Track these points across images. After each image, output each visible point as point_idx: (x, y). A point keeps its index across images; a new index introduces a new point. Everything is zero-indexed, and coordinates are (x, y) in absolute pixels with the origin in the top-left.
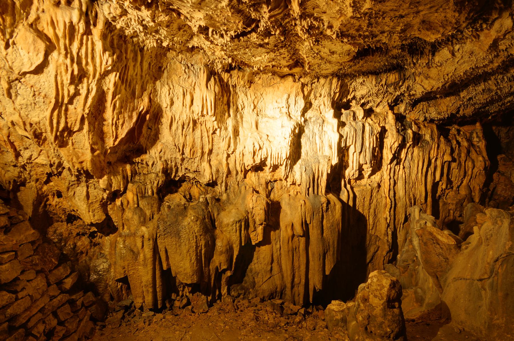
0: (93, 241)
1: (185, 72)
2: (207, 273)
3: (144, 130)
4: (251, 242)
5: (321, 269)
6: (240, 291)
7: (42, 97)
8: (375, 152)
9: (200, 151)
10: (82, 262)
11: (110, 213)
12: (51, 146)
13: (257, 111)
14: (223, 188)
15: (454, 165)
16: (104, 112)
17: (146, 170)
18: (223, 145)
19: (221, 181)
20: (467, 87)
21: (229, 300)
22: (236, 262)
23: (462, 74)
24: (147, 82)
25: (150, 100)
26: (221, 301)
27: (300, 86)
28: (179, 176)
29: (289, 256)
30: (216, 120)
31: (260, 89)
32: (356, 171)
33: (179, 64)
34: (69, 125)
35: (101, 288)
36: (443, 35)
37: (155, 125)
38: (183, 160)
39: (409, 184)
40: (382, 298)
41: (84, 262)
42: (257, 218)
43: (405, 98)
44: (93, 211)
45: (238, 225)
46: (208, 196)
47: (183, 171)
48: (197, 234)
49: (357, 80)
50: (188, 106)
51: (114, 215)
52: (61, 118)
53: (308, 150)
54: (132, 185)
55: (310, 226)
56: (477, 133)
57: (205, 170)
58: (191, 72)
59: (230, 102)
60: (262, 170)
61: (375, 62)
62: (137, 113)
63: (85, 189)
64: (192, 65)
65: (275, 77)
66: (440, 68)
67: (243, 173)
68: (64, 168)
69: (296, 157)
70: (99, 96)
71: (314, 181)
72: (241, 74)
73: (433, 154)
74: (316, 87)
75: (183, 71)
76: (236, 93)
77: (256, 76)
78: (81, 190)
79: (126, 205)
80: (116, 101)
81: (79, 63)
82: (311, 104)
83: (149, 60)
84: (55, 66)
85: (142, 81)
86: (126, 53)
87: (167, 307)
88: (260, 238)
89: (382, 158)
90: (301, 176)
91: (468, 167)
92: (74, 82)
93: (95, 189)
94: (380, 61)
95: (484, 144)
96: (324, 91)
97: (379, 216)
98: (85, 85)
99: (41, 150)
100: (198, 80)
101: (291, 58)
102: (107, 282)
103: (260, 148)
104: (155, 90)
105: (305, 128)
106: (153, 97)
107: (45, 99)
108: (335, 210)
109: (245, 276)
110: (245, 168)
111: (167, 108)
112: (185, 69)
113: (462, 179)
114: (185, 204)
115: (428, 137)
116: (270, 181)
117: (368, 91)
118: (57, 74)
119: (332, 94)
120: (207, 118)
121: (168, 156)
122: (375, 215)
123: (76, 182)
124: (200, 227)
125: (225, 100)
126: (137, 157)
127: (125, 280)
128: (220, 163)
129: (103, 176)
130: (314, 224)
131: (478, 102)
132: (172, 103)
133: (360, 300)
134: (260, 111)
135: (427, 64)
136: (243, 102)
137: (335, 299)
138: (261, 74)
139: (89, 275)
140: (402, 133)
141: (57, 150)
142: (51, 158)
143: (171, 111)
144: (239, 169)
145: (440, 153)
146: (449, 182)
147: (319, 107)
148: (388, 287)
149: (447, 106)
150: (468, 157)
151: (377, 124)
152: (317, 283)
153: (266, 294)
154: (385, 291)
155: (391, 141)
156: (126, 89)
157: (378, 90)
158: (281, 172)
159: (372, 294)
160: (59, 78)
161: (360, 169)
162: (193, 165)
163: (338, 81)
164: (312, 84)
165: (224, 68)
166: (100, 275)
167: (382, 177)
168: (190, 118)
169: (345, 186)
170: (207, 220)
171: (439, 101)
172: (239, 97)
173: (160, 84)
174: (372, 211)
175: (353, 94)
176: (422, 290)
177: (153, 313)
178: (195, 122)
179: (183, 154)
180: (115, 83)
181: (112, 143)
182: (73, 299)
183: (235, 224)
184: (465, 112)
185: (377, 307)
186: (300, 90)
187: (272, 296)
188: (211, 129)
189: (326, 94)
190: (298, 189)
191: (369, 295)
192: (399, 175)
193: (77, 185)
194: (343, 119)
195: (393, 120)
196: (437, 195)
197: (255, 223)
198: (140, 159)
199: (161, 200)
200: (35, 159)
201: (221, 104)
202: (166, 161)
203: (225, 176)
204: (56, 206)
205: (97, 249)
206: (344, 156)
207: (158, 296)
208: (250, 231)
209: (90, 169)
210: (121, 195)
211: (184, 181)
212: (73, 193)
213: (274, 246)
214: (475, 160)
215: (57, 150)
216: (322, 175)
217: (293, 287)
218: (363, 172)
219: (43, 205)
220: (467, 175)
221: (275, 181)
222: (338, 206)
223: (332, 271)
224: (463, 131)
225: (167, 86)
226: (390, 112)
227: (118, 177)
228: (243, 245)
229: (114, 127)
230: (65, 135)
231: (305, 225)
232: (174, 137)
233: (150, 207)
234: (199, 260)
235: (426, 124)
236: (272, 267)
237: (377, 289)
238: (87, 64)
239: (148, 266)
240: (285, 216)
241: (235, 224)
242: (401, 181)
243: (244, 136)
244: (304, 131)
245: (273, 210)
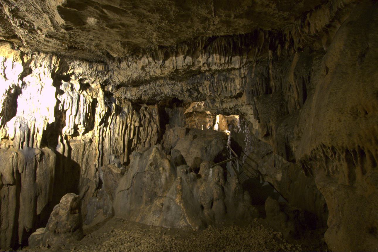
5: (31, 211)
15: (141, 129)
27: (19, 54)
39: (113, 140)
40: (67, 208)
49: (75, 62)
55: (23, 175)
56: (155, 111)
71: (28, 136)
73: (129, 121)
89: (94, 121)
97: (90, 163)
108: (49, 159)
115: (126, 110)
130: (27, 173)
146: (139, 139)
155: (101, 109)
161: (76, 128)
167: (93, 134)
169: (62, 141)
174: (85, 160)
194: (62, 88)
196: (132, 148)
216: (38, 131)
222: (52, 156)
235: (126, 101)
242: (108, 138)
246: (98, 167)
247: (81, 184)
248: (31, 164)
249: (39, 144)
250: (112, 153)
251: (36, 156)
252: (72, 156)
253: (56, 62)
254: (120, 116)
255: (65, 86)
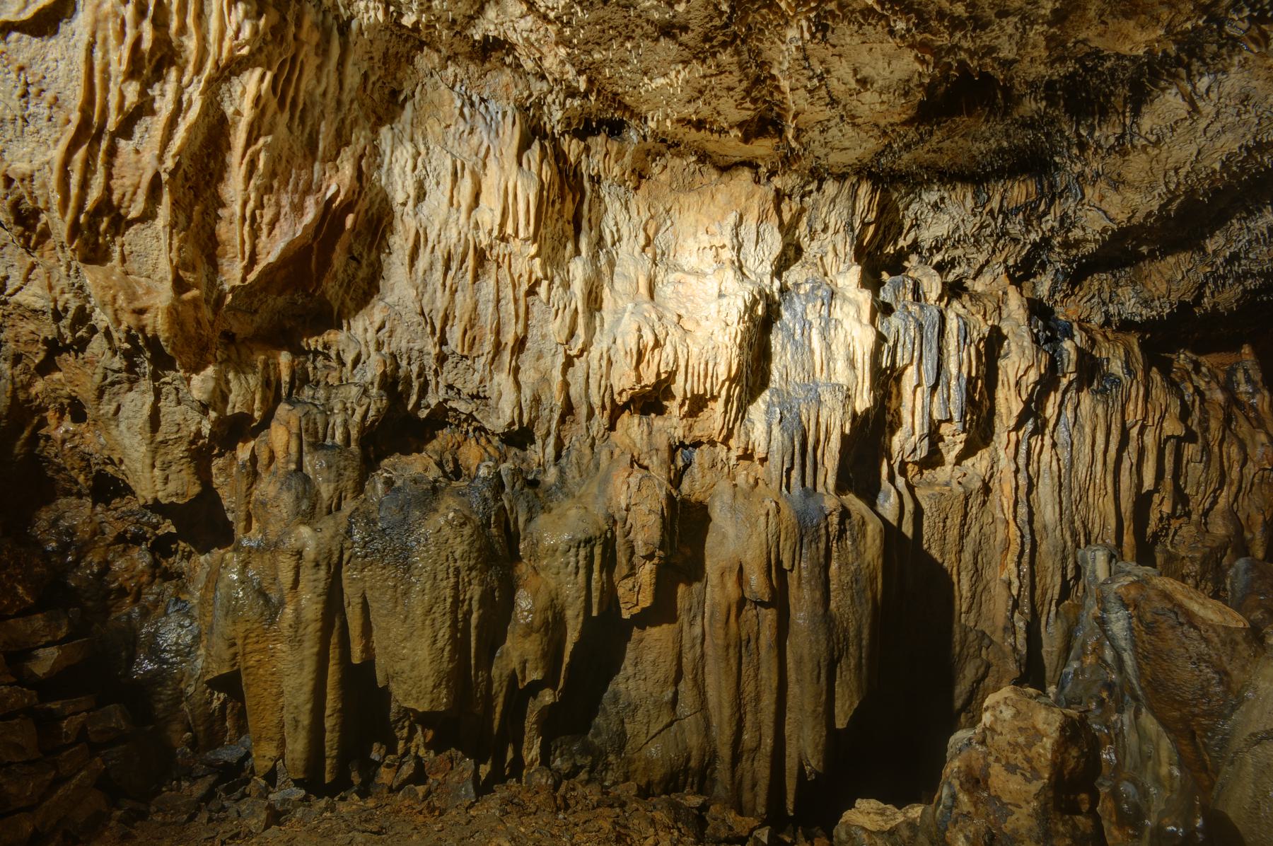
0: (164, 564)
1: (462, 114)
2: (482, 686)
3: (339, 258)
4: (619, 609)
5: (820, 709)
6: (578, 757)
7: (45, 104)
8: (975, 391)
9: (490, 338)
10: (118, 619)
11: (218, 480)
12: (60, 254)
13: (655, 255)
14: (550, 450)
15: (1190, 450)
16: (221, 179)
17: (335, 374)
18: (555, 328)
19: (544, 431)
20: (1225, 224)
21: (544, 780)
22: (570, 665)
23: (1217, 166)
24: (355, 122)
25: (359, 175)
26: (519, 781)
27: (771, 195)
28: (428, 406)
29: (728, 660)
30: (538, 254)
31: (664, 196)
32: (921, 440)
33: (447, 91)
34: (115, 198)
35: (160, 701)
36: (1169, 29)
37: (370, 251)
38: (442, 359)
39: (1071, 491)
40: (1036, 775)
41: (124, 618)
42: (639, 537)
43: (1054, 257)
44: (166, 466)
45: (582, 553)
46: (505, 467)
47: (442, 392)
48: (459, 563)
49: (924, 196)
50: (464, 208)
51: (227, 489)
52: (94, 172)
53: (791, 366)
54: (287, 407)
55: (792, 578)
56: (1246, 371)
57: (501, 395)
58: (478, 117)
59: (582, 217)
60: (661, 411)
61: (975, 139)
62: (317, 203)
63: (150, 398)
64: (482, 100)
65: (704, 169)
66: (1157, 151)
67: (607, 413)
68: (93, 330)
69: (754, 383)
70: (211, 128)
71: (803, 450)
72: (614, 146)
73: (1134, 412)
74: (815, 206)
75: (457, 112)
76: (601, 200)
77: (654, 160)
78: (137, 402)
79: (266, 462)
80: (258, 152)
81: (160, 24)
82: (799, 251)
83: (365, 66)
84: (90, 19)
85: (341, 116)
86: (299, 25)
87: (351, 784)
88: (646, 600)
89: (992, 411)
90: (770, 432)
91: (1229, 458)
92: (140, 73)
93: (179, 403)
94: (987, 134)
95: (1267, 399)
96: (836, 218)
97: (988, 574)
98: (170, 88)
99: (33, 267)
100: (496, 142)
101: (748, 91)
102: (183, 686)
103: (657, 344)
104: (376, 151)
105: (782, 308)
106: (369, 167)
107: (55, 109)
108: (864, 536)
109: (596, 714)
110: (613, 400)
111: (404, 204)
112: (463, 105)
113: (1215, 491)
114: (436, 481)
115: (1116, 367)
116: (682, 444)
117: (952, 226)
118: (95, 42)
119: (857, 224)
120: (515, 245)
121: (400, 342)
122: (977, 573)
123: (124, 375)
124: (471, 544)
125: (567, 210)
126: (312, 336)
127: (230, 684)
128: (545, 379)
129: (204, 368)
130: (804, 573)
131: (1256, 269)
132: (421, 195)
133: (956, 783)
134: (663, 254)
135: (1117, 139)
136: (616, 224)
137: (866, 796)
138: (668, 156)
139: (131, 660)
140: (1046, 347)
141: (77, 270)
142: (57, 290)
143: (416, 215)
144: (596, 400)
145: (1154, 414)
146: (1180, 497)
147: (821, 259)
148: (1056, 735)
149: (1168, 282)
150: (1227, 432)
151: (980, 317)
152: (809, 751)
153: (657, 775)
154: (1047, 745)
155: (1018, 365)
156: (290, 128)
157: (981, 227)
158: (714, 418)
159: (997, 760)
160: (98, 54)
161: (934, 435)
162: (468, 377)
163: (874, 191)
164: (802, 197)
165: (569, 125)
166: (165, 661)
167: (994, 463)
168: (467, 240)
169: (892, 479)
170: (494, 530)
171: (1146, 267)
172: (606, 210)
173: (390, 136)
174: (967, 556)
175: (912, 234)
176: (1136, 785)
177: (303, 792)
178: (481, 257)
179: (443, 341)
180: (258, 99)
181: (239, 276)
182: (50, 710)
183: (573, 550)
184: (1218, 298)
185: (1019, 806)
186: (770, 206)
187: (673, 781)
188: (526, 277)
189: (841, 225)
190: (760, 470)
191: (988, 765)
192: (1042, 465)
193: (126, 386)
194: (886, 295)
195: (1022, 311)
196: (1149, 531)
197: (633, 553)
198: (320, 340)
199: (369, 465)
200: (16, 291)
201: (555, 216)
202: (393, 356)
203: (556, 416)
204: (64, 442)
205: (170, 588)
206: (887, 395)
207: (327, 744)
208: (616, 577)
209: (163, 336)
210: (255, 433)
211: (444, 425)
212: (114, 405)
213: (686, 627)
214: (1248, 442)
215: (77, 270)
216: (827, 439)
217: (736, 758)
218: (941, 445)
219: (26, 434)
220: (1228, 480)
221: (697, 444)
222: (873, 527)
223: (857, 718)
224: (1208, 364)
225: (409, 146)
226: (1012, 291)
227: (249, 377)
228: (595, 613)
229: (247, 228)
230: (103, 226)
231: (777, 573)
232: (421, 288)
233: (332, 476)
234: (459, 643)
235: (1109, 335)
236: (676, 694)
237: (1017, 744)
238: (183, 30)
239: (307, 644)
240: (721, 543)
241: (573, 550)
242: (1048, 481)
243: (616, 312)
244: (779, 316)
245: (686, 523)
246: (1019, 595)
247: (958, 649)
248: (813, 546)
249: (831, 482)
250: (1069, 544)
251: (826, 517)
252: (926, 537)
253: (870, 203)
254: (1095, 392)
255: (896, 288)
